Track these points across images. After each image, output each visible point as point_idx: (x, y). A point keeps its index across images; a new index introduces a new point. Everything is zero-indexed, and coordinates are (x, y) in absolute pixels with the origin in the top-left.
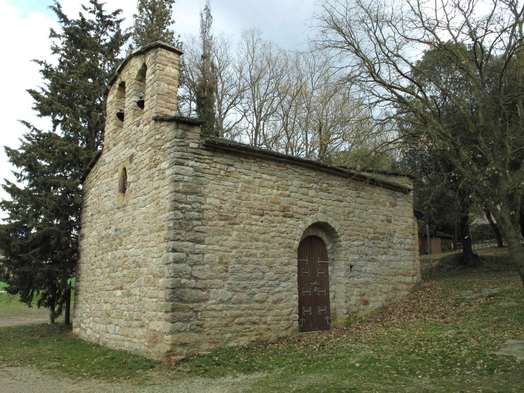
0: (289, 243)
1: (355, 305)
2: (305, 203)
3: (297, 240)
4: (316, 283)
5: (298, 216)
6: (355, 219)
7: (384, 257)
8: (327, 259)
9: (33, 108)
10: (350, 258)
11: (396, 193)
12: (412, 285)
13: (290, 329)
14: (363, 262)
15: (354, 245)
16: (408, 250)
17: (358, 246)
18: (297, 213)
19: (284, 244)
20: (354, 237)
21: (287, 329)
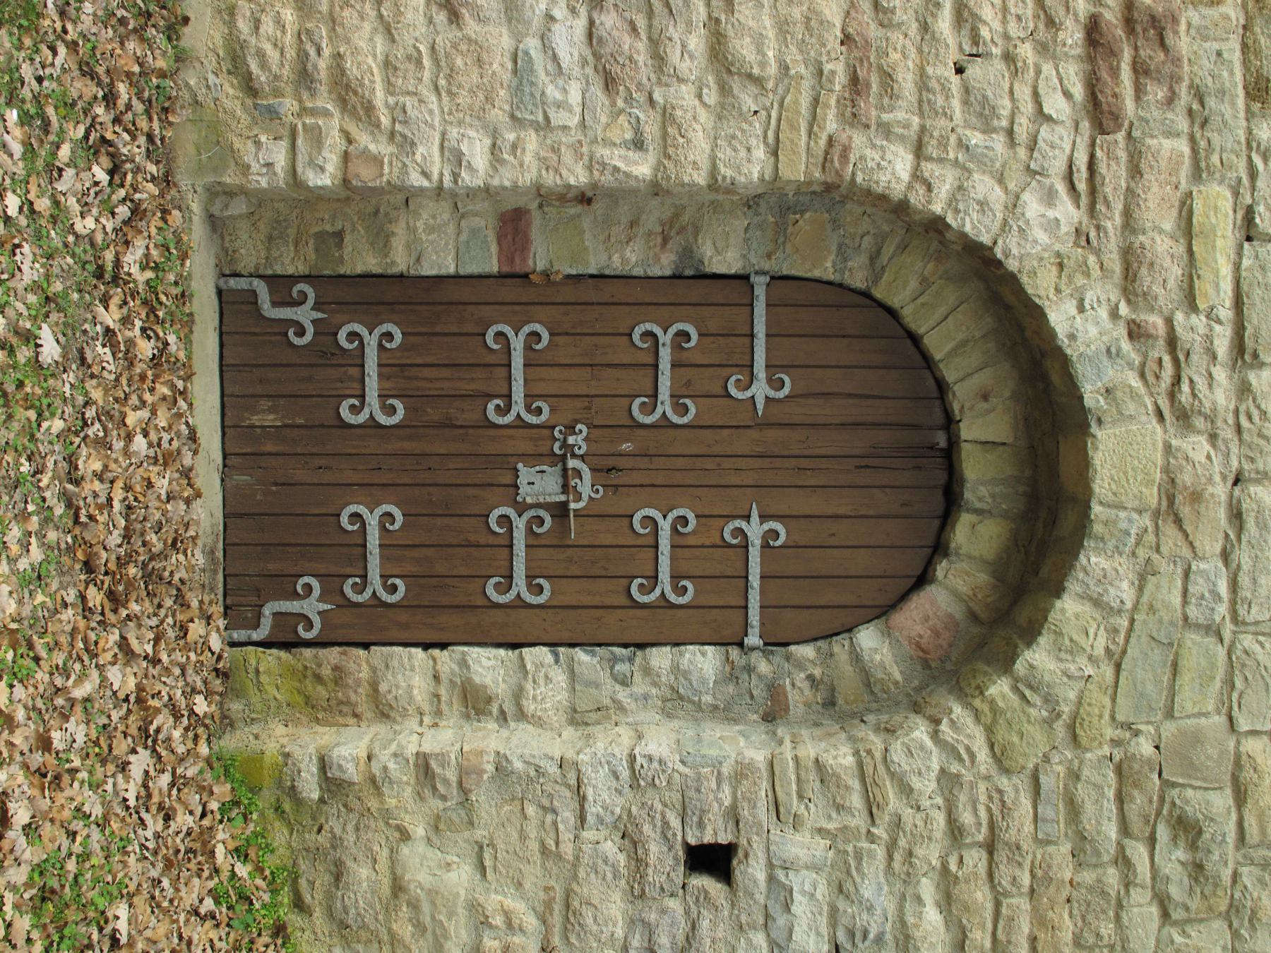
0: (887, 77)
1: (398, 887)
2: (1226, 270)
3: (916, 175)
4: (585, 488)
5: (1114, 175)
8: (775, 643)
10: (801, 846)
13: (229, 91)
15: (907, 897)
18: (1135, 171)
19: (874, 31)
20: (981, 896)
21: (235, 59)
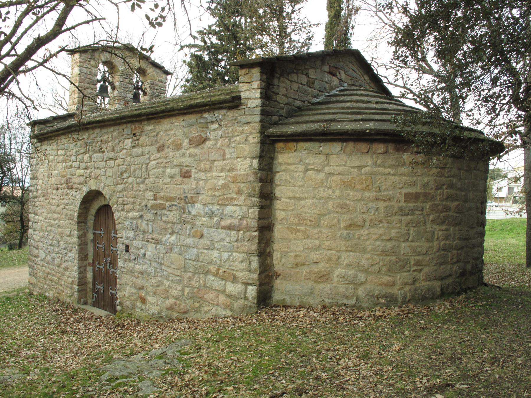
6: (131, 180)
7: (173, 238)
9: (389, 43)
11: (206, 115)
12: (242, 302)
14: (140, 243)
16: (230, 228)
17: (133, 219)
